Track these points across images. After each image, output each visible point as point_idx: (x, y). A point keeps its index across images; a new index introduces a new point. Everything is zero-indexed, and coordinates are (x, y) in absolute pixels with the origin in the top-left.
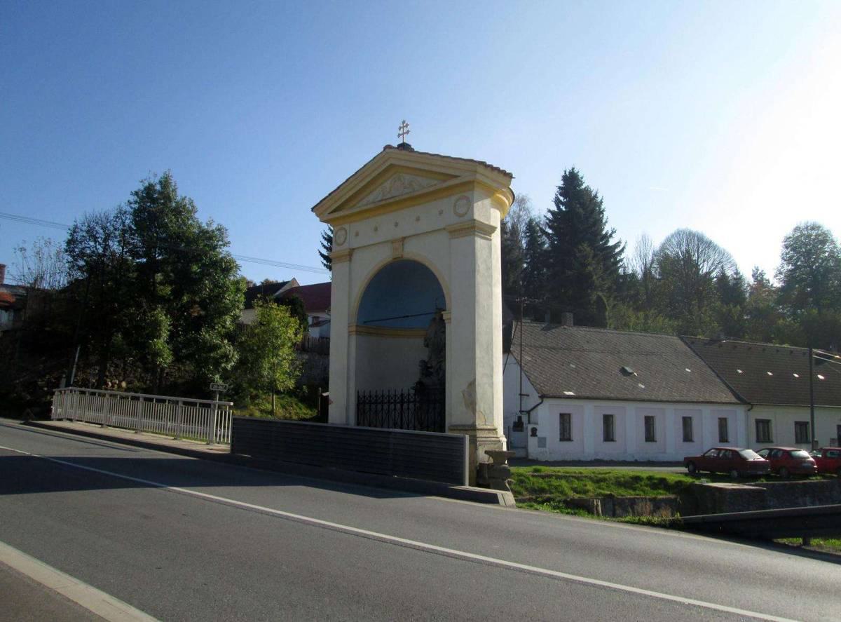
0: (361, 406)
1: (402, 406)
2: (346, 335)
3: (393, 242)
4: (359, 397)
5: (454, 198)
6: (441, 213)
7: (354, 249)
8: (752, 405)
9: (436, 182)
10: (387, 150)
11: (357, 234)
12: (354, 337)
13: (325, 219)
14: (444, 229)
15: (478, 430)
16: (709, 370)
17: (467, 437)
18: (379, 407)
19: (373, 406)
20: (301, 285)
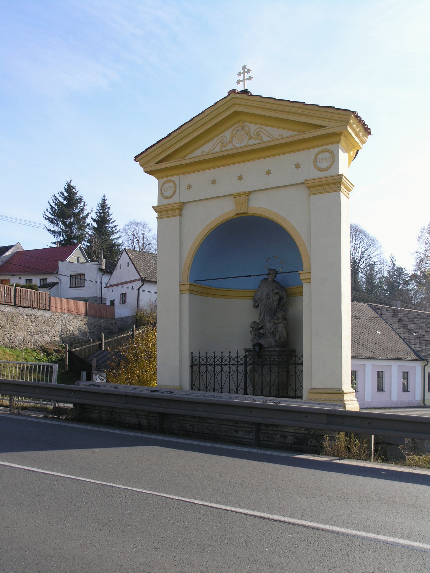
0: (195, 368)
1: (246, 368)
2: (177, 292)
3: (236, 196)
4: (192, 358)
5: (314, 151)
6: (297, 166)
7: (185, 203)
8: (428, 362)
9: (295, 133)
10: (232, 95)
11: (189, 187)
12: (186, 296)
13: (145, 171)
14: (302, 183)
15: (345, 393)
16: (393, 333)
17: (54, 382)
18: (234, 368)
19: (226, 368)
20: (25, 250)
